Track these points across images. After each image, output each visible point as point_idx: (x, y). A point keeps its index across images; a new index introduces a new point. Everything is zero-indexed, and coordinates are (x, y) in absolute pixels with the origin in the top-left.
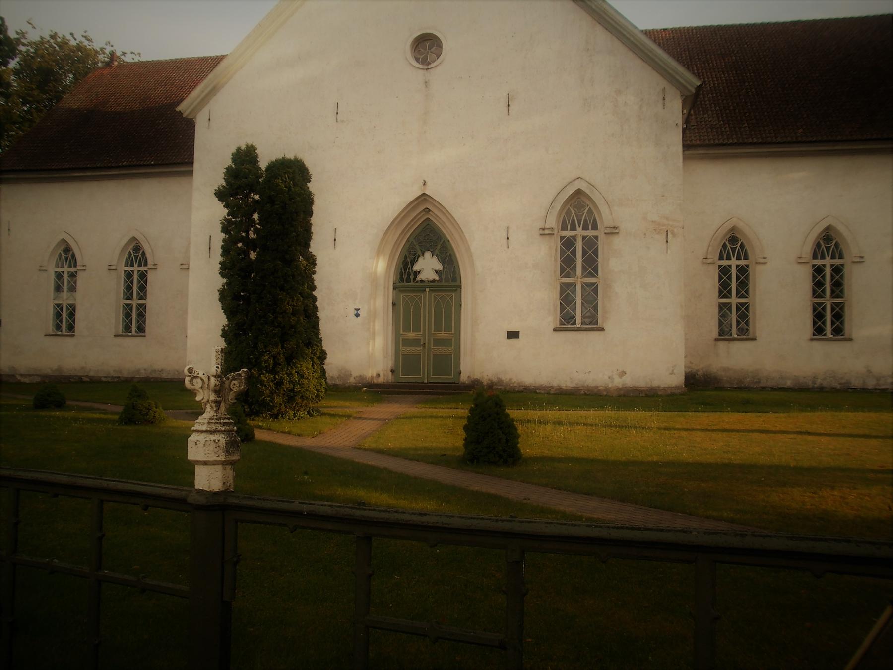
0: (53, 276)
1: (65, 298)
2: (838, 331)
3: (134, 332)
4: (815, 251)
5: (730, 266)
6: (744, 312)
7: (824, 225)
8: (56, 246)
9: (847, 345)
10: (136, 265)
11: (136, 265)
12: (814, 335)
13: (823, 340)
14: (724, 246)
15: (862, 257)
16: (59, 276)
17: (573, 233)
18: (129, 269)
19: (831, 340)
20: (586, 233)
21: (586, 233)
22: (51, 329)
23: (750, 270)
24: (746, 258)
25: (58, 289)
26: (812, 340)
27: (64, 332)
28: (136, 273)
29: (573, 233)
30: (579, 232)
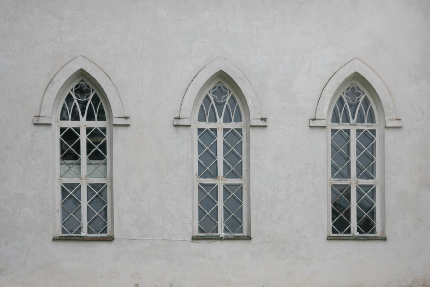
0: (58, 136)
1: (85, 173)
2: (367, 225)
3: (84, 233)
4: (335, 111)
5: (78, 130)
6: (236, 198)
7: (347, 73)
8: (66, 82)
9: (378, 245)
10: (220, 120)
11: (220, 120)
12: (334, 231)
13: (348, 239)
14: (69, 98)
15: (264, 120)
16: (70, 136)
17: (212, 125)
18: (342, 126)
19: (356, 239)
20: (360, 127)
21: (360, 127)
22: (193, 225)
23: (377, 139)
24: (102, 117)
25: (69, 155)
26: (329, 238)
27: (84, 233)
28: (220, 133)
29: (212, 125)
30: (220, 125)
